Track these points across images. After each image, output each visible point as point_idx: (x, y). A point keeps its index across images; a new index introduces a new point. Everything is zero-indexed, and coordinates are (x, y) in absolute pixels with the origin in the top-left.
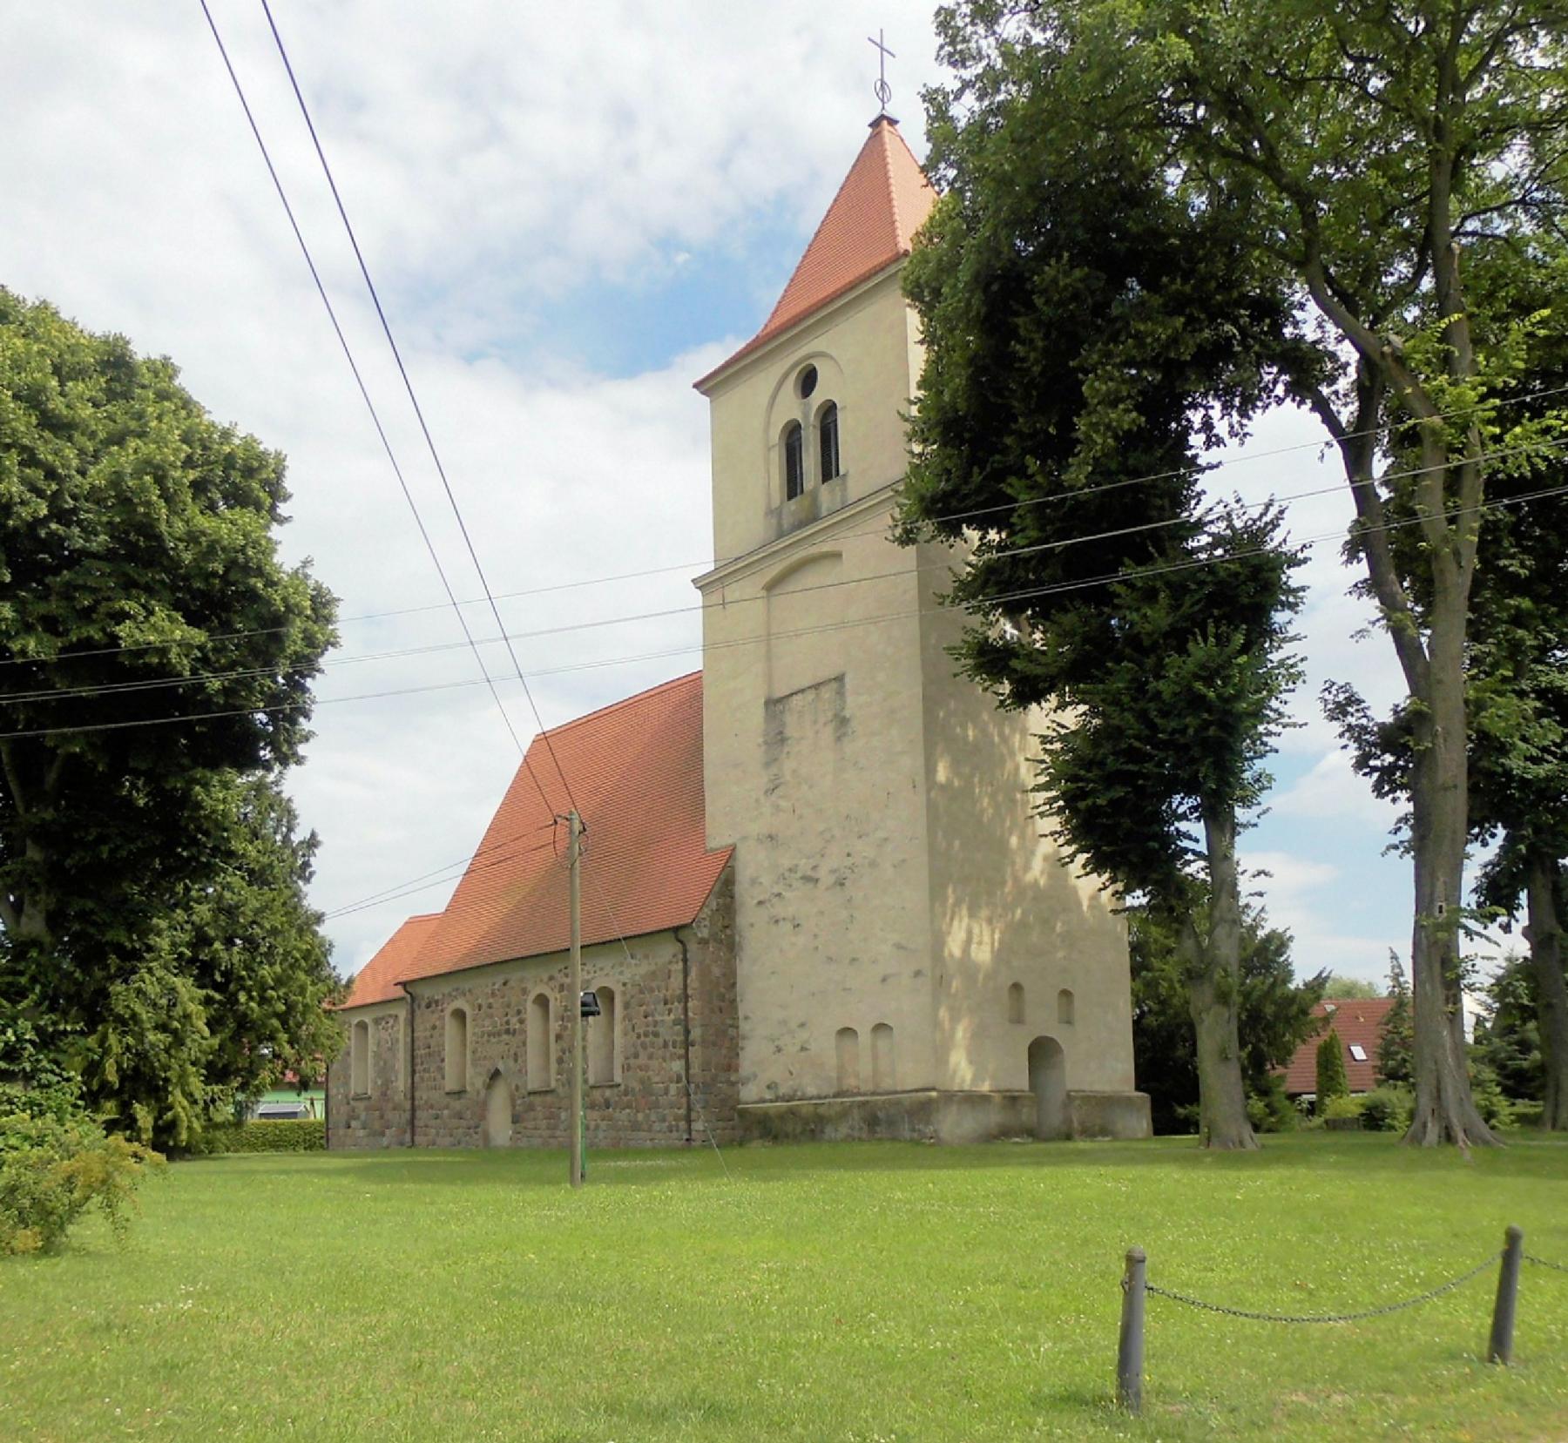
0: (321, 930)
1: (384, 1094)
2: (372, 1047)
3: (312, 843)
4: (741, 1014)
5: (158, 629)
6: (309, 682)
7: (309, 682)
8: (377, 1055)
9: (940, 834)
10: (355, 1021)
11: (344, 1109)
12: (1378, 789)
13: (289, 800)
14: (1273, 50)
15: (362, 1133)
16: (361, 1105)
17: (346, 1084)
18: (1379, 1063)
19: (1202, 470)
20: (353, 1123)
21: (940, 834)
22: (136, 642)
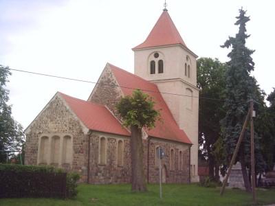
0: (252, 56)
1: (110, 164)
2: (106, 147)
3: (237, 24)
4: (196, 94)
5: (251, 64)
6: (235, 37)
7: (235, 37)
8: (108, 151)
9: (220, 173)
10: (101, 136)
11: (95, 168)
12: (228, 47)
13: (237, 24)
14: (35, 134)
15: (102, 178)
16: (102, 168)
17: (96, 159)
18: (76, 189)
19: (111, 162)
20: (99, 174)
21: (220, 173)
22: (263, 97)
